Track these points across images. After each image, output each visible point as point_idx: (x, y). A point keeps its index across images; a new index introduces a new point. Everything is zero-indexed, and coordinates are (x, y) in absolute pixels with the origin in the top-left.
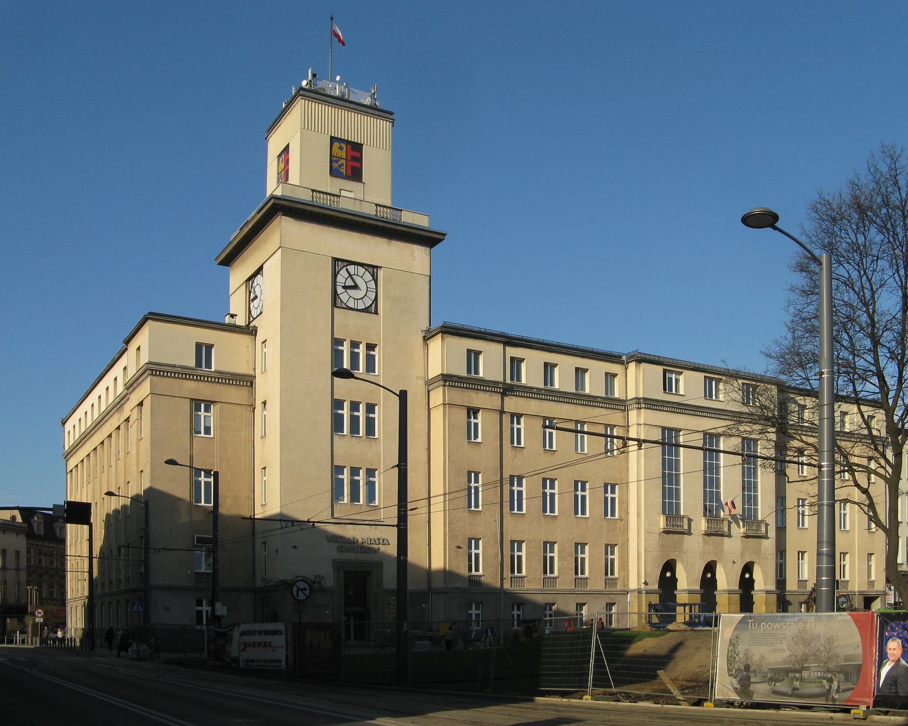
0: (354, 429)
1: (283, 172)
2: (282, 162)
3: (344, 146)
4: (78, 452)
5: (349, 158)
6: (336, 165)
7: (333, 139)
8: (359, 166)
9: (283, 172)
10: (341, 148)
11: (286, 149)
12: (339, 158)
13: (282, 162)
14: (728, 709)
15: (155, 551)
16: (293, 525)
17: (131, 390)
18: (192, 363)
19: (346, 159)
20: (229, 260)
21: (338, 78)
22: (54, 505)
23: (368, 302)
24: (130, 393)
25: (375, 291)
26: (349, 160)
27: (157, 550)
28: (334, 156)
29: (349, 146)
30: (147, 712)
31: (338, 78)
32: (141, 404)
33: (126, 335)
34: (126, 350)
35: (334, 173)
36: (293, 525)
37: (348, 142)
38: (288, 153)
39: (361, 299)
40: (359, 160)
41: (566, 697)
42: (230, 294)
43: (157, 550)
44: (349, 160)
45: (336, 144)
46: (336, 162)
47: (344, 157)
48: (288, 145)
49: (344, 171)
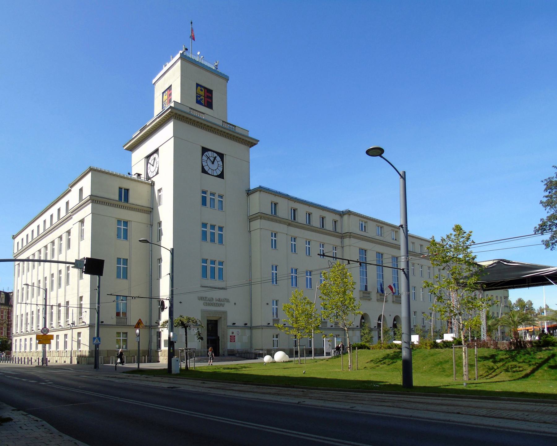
0: (213, 240)
1: (167, 100)
2: (166, 95)
3: (203, 89)
4: (24, 253)
5: (206, 96)
6: (199, 99)
7: (198, 85)
8: (211, 101)
9: (167, 100)
10: (201, 90)
11: (170, 88)
12: (201, 95)
13: (166, 95)
14: (554, 400)
15: (133, 298)
16: (349, 263)
17: (73, 213)
18: (117, 198)
19: (204, 97)
20: (132, 148)
21: (199, 53)
22: (76, 260)
23: (219, 173)
24: (73, 215)
25: (222, 167)
26: (206, 97)
27: (134, 298)
28: (198, 94)
29: (206, 90)
30: (225, 420)
31: (199, 53)
32: (82, 221)
33: (72, 181)
34: (70, 191)
35: (198, 102)
36: (349, 263)
37: (205, 88)
38: (171, 89)
39: (215, 170)
40: (211, 98)
41: (130, 370)
42: (132, 166)
43: (134, 298)
44: (206, 97)
45: (199, 88)
46: (199, 97)
47: (203, 95)
48: (171, 86)
49: (203, 102)
